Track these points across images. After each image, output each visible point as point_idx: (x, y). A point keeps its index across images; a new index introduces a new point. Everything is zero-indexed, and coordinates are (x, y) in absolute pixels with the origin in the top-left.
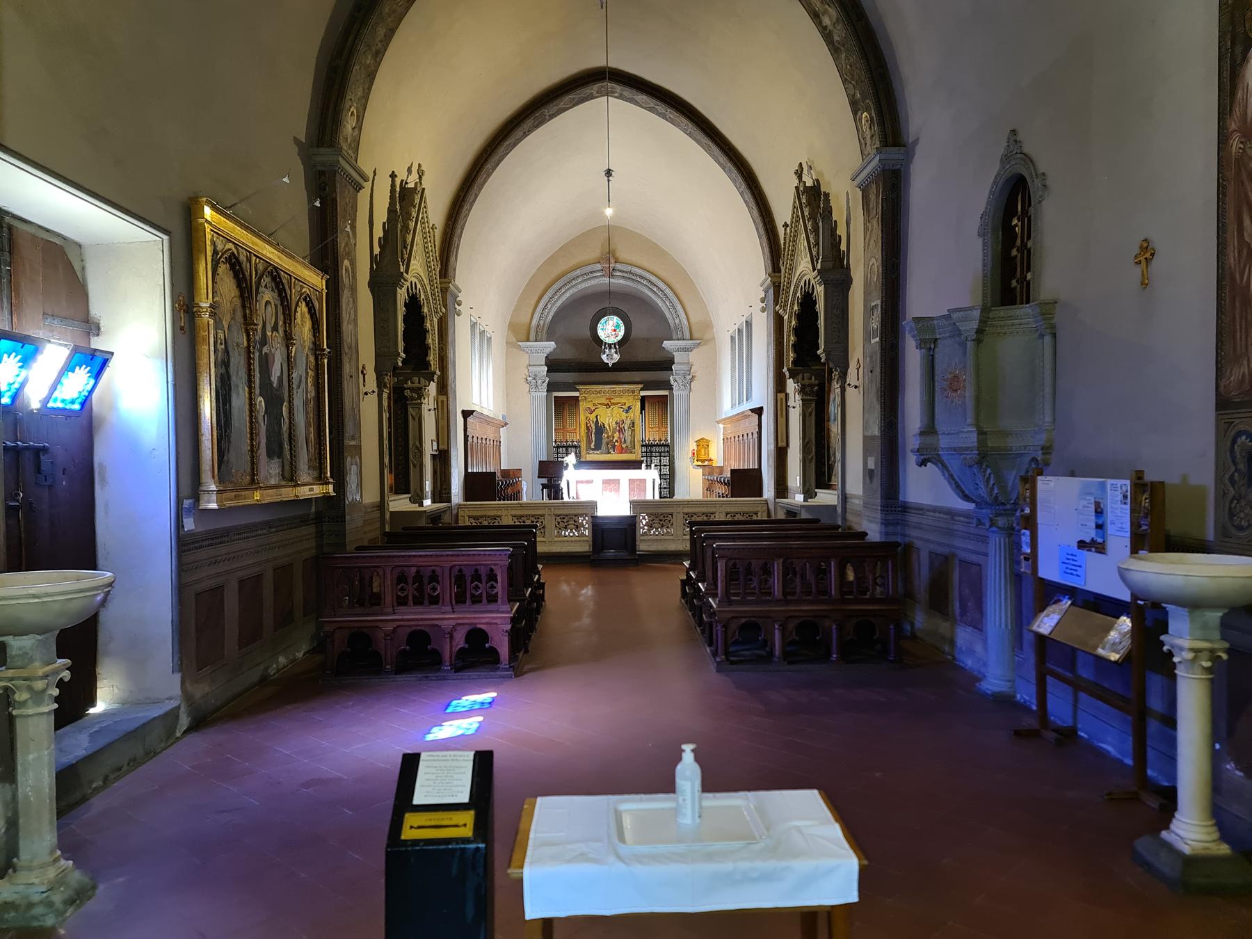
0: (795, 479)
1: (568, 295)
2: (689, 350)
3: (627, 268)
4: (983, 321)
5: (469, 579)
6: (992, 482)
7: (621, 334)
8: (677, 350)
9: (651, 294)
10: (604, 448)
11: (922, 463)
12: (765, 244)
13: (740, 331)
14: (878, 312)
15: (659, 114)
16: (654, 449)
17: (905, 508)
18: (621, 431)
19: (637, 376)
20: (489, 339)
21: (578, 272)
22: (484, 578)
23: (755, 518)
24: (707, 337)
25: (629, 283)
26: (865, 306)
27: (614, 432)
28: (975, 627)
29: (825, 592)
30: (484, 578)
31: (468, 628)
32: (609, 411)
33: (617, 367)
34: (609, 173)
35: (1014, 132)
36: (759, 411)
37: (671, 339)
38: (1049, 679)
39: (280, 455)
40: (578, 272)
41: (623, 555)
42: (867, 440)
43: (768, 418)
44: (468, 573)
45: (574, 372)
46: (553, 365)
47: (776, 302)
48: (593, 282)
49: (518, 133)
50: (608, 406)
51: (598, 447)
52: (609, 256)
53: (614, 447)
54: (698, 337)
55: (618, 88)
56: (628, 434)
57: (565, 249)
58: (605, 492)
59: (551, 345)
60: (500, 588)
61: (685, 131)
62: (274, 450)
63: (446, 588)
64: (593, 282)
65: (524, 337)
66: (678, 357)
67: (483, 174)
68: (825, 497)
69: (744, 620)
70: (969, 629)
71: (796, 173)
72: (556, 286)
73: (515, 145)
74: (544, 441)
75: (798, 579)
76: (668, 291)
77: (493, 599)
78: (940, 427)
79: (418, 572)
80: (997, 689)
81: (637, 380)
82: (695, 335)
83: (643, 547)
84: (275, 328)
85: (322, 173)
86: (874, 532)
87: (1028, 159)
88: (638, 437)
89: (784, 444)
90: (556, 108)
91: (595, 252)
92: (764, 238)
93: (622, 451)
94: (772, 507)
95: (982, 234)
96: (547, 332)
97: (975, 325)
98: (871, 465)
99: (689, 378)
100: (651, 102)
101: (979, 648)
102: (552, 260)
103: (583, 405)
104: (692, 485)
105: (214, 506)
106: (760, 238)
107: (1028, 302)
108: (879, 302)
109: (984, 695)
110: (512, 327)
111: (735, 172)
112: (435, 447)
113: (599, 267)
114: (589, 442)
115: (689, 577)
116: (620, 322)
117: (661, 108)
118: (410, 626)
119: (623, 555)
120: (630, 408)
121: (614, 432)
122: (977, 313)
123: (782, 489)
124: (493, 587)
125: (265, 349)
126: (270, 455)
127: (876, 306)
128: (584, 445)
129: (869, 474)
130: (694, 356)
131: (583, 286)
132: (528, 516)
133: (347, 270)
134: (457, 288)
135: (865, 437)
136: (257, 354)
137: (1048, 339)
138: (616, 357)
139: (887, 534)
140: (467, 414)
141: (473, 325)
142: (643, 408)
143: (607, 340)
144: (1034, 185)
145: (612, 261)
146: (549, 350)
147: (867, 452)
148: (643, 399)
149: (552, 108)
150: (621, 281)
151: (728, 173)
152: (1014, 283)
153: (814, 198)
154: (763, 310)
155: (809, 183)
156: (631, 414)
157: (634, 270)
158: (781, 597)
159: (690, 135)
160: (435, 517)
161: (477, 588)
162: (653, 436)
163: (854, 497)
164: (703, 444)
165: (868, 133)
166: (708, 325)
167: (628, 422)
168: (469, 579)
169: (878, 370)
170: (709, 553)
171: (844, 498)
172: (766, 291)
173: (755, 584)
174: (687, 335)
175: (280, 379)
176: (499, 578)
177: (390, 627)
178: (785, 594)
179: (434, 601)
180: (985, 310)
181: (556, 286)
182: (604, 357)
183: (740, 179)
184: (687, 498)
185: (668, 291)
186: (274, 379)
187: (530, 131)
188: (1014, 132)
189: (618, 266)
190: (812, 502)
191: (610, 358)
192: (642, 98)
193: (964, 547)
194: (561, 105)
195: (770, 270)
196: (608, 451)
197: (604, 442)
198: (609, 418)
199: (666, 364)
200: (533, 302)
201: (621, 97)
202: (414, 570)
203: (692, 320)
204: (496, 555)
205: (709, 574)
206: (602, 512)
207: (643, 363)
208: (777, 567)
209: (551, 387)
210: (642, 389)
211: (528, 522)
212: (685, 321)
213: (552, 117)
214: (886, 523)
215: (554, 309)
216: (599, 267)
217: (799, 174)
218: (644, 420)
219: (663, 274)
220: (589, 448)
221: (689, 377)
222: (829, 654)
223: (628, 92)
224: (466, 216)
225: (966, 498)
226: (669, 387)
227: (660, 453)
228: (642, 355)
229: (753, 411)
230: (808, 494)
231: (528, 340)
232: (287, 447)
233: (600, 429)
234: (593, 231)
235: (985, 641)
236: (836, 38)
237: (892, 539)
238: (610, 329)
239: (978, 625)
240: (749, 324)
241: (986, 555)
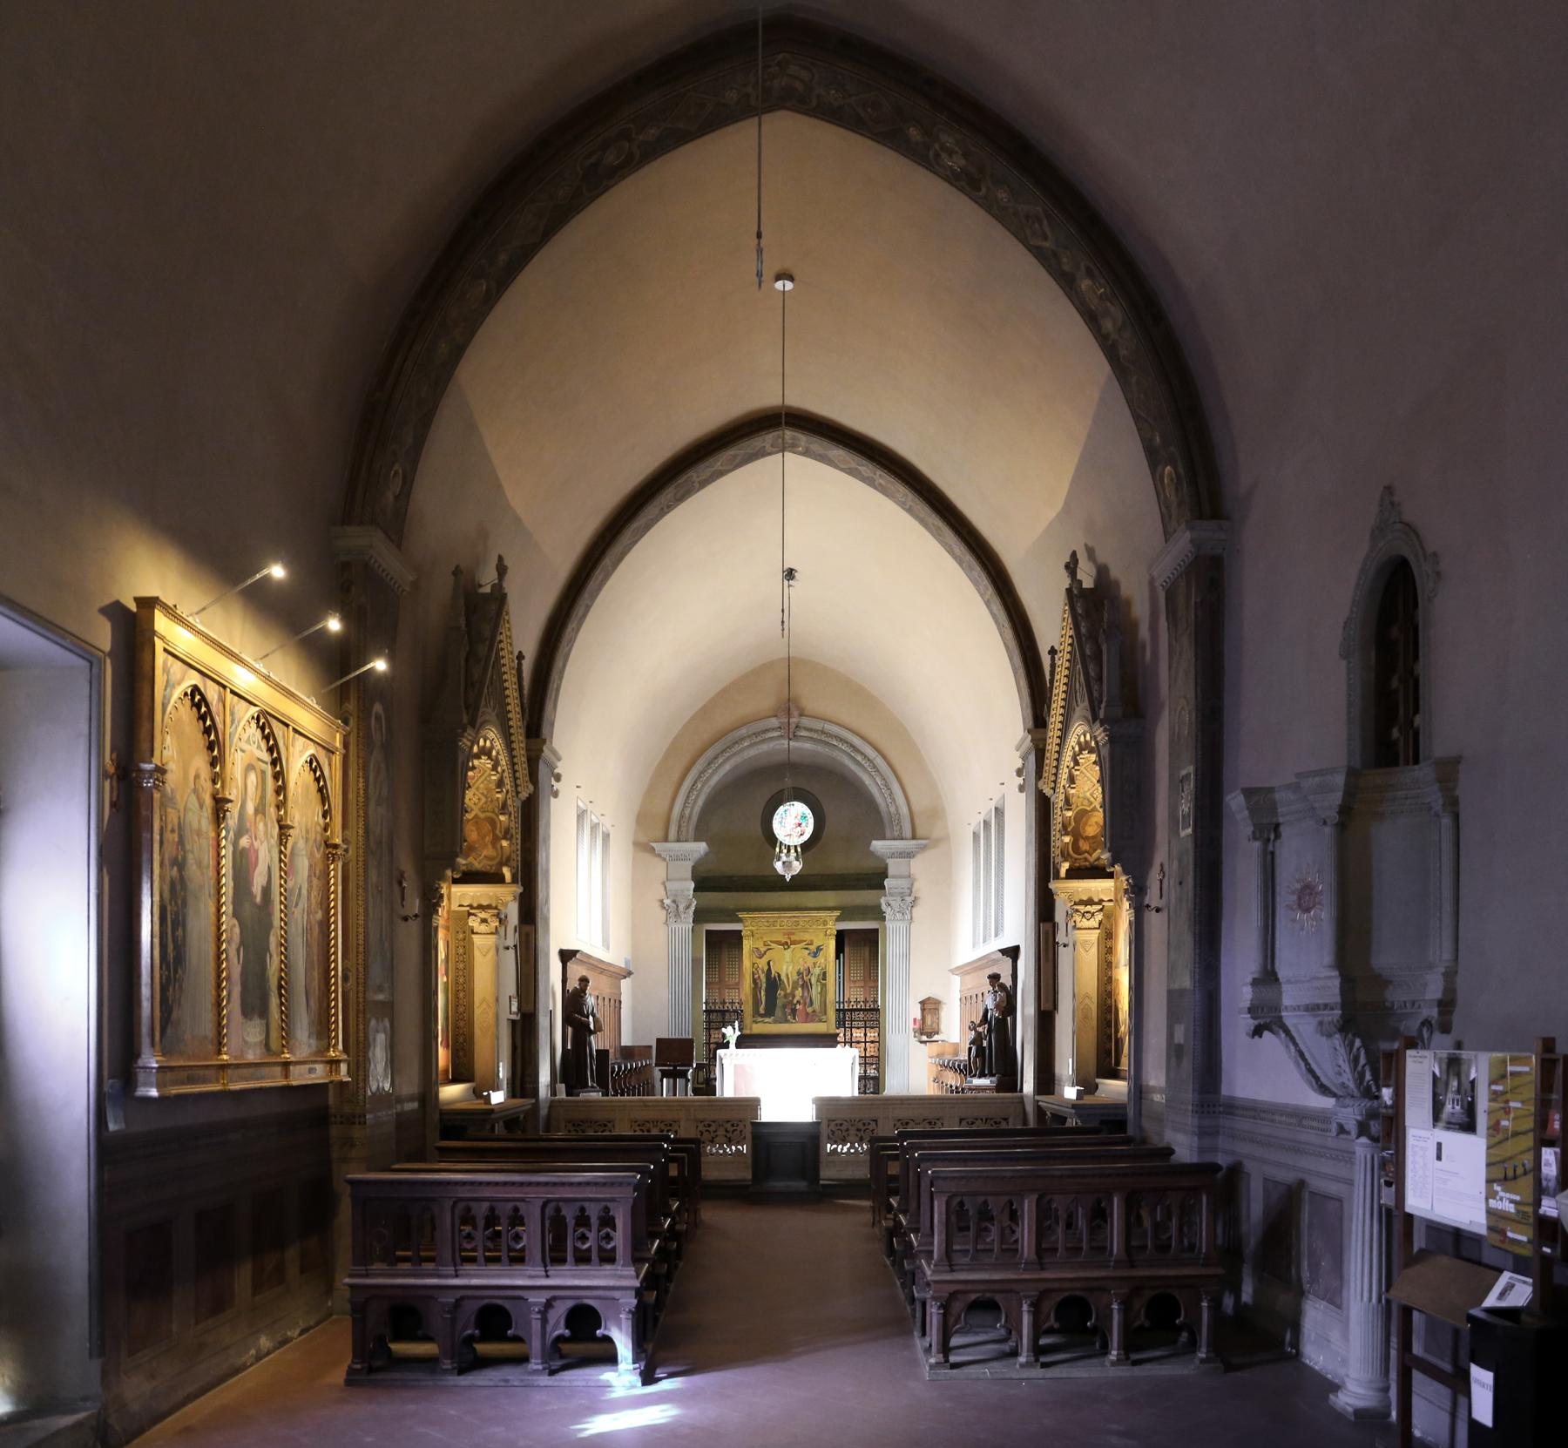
0: (1065, 1066)
1: (727, 767)
2: (909, 855)
3: (818, 725)
4: (1350, 792)
5: (571, 1223)
6: (1362, 1060)
7: (809, 830)
8: (892, 856)
9: (853, 767)
10: (778, 1012)
11: (1258, 1032)
12: (1023, 683)
13: (986, 824)
14: (1190, 786)
15: (864, 480)
16: (855, 1015)
17: (1232, 1107)
18: (806, 986)
19: (831, 897)
20: (606, 837)
21: (743, 731)
22: (594, 1221)
23: (1003, 1126)
24: (937, 833)
25: (820, 748)
26: (1171, 776)
27: (794, 988)
28: (1331, 1302)
29: (1101, 1249)
30: (594, 1221)
31: (570, 1304)
32: (788, 953)
33: (800, 884)
34: (790, 574)
35: (1389, 490)
36: (1013, 953)
37: (884, 838)
38: (1417, 1376)
39: (264, 1013)
40: (743, 731)
41: (801, 1185)
42: (1173, 996)
43: (1026, 965)
44: (569, 1213)
45: (727, 887)
46: (704, 882)
47: (1039, 774)
48: (765, 747)
49: (651, 510)
50: (786, 945)
51: (770, 1012)
52: (789, 707)
53: (794, 1011)
54: (923, 833)
55: (803, 439)
56: (815, 991)
57: (726, 694)
58: (785, 1084)
59: (701, 847)
60: (620, 1239)
61: (902, 505)
62: (255, 1006)
63: (531, 1237)
64: (765, 747)
65: (660, 833)
66: (894, 867)
67: (598, 574)
68: (1114, 1089)
69: (973, 1297)
70: (1322, 1305)
71: (1067, 566)
72: (710, 754)
73: (648, 528)
74: (687, 1001)
75: (1060, 1230)
76: (879, 761)
77: (608, 1258)
78: (1283, 972)
79: (492, 1209)
80: (1361, 1404)
81: (832, 904)
82: (920, 832)
83: (827, 1174)
84: (260, 810)
85: (346, 566)
86: (1185, 1149)
87: (1410, 529)
88: (831, 995)
89: (1049, 1007)
90: (708, 472)
91: (764, 701)
92: (1021, 672)
93: (808, 1018)
94: (1030, 1108)
95: (1346, 654)
96: (697, 828)
97: (1337, 798)
98: (1179, 1037)
99: (910, 900)
100: (960, 548)
101: (1335, 1335)
102: (706, 711)
103: (747, 945)
104: (915, 1073)
105: (154, 1093)
106: (1015, 673)
107: (1416, 762)
108: (1191, 769)
109: (1338, 1416)
110: (642, 819)
111: (978, 570)
112: (514, 1009)
113: (774, 722)
114: (756, 1002)
115: (898, 1224)
116: (808, 812)
117: (867, 468)
118: (482, 1298)
119: (801, 1185)
120: (819, 949)
121: (794, 988)
122: (1340, 780)
123: (1046, 1080)
124: (608, 1238)
125: (244, 842)
126: (247, 1012)
127: (1188, 775)
128: (748, 1009)
129: (1175, 1052)
130: (917, 866)
131: (753, 752)
132: (655, 1123)
133: (378, 718)
134: (555, 753)
135: (1170, 992)
136: (231, 849)
137: (1446, 821)
138: (797, 867)
139: (1201, 1150)
140: (566, 956)
141: (581, 815)
142: (839, 950)
143: (787, 841)
144: (1421, 570)
145: (796, 713)
146: (696, 856)
147: (1173, 1018)
148: (841, 937)
149: (703, 470)
150: (808, 746)
151: (967, 570)
152: (1395, 733)
153: (1093, 605)
154: (1022, 788)
155: (1088, 583)
156: (821, 959)
157: (829, 727)
158: (1033, 1257)
159: (909, 510)
160: (511, 1120)
161: (584, 1238)
162: (855, 995)
163: (1154, 1090)
164: (930, 1006)
165: (1173, 499)
166: (937, 813)
167: (817, 971)
168: (571, 1223)
169: (1190, 881)
170: (925, 1183)
171: (1139, 1091)
172: (1024, 758)
173: (993, 1235)
174: (907, 832)
175: (267, 891)
176: (619, 1223)
177: (450, 1299)
178: (1039, 1251)
179: (518, 1259)
180: (1352, 773)
181: (710, 754)
182: (778, 866)
183: (985, 581)
184: (904, 1093)
185: (879, 761)
186: (257, 889)
187: (670, 508)
188: (1389, 490)
189: (805, 722)
190: (1088, 1100)
191: (788, 866)
192: (838, 453)
193: (1321, 1175)
194: (718, 466)
195: (1030, 724)
196: (778, 1018)
197: (779, 1002)
198: (787, 965)
199: (875, 879)
200: (676, 777)
201: (807, 453)
202: (486, 1205)
203: (916, 807)
204: (604, 1186)
205: (913, 1205)
206: (767, 1115)
207: (841, 876)
208: (1028, 1208)
209: (700, 916)
210: (838, 919)
211: (655, 1132)
212: (904, 810)
213: (704, 483)
214: (1203, 1133)
215: (707, 790)
216: (774, 722)
217: (1071, 567)
218: (840, 969)
219: (873, 735)
220: (756, 1013)
221: (909, 899)
222: (1105, 1350)
223: (818, 444)
224: (572, 641)
225: (1324, 1090)
226: (879, 914)
227: (860, 1018)
228: (840, 863)
229: (1004, 952)
230: (1088, 1087)
231: (666, 840)
232: (274, 1001)
233: (773, 983)
234: (768, 667)
235: (1345, 1324)
236: (1123, 352)
237: (1208, 1158)
238: (792, 823)
239: (1335, 1298)
240: (999, 812)
241: (1350, 1183)
